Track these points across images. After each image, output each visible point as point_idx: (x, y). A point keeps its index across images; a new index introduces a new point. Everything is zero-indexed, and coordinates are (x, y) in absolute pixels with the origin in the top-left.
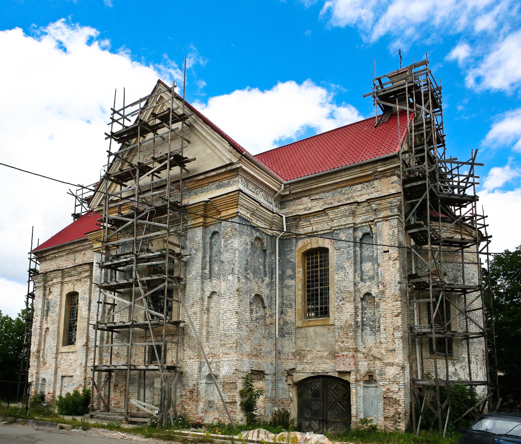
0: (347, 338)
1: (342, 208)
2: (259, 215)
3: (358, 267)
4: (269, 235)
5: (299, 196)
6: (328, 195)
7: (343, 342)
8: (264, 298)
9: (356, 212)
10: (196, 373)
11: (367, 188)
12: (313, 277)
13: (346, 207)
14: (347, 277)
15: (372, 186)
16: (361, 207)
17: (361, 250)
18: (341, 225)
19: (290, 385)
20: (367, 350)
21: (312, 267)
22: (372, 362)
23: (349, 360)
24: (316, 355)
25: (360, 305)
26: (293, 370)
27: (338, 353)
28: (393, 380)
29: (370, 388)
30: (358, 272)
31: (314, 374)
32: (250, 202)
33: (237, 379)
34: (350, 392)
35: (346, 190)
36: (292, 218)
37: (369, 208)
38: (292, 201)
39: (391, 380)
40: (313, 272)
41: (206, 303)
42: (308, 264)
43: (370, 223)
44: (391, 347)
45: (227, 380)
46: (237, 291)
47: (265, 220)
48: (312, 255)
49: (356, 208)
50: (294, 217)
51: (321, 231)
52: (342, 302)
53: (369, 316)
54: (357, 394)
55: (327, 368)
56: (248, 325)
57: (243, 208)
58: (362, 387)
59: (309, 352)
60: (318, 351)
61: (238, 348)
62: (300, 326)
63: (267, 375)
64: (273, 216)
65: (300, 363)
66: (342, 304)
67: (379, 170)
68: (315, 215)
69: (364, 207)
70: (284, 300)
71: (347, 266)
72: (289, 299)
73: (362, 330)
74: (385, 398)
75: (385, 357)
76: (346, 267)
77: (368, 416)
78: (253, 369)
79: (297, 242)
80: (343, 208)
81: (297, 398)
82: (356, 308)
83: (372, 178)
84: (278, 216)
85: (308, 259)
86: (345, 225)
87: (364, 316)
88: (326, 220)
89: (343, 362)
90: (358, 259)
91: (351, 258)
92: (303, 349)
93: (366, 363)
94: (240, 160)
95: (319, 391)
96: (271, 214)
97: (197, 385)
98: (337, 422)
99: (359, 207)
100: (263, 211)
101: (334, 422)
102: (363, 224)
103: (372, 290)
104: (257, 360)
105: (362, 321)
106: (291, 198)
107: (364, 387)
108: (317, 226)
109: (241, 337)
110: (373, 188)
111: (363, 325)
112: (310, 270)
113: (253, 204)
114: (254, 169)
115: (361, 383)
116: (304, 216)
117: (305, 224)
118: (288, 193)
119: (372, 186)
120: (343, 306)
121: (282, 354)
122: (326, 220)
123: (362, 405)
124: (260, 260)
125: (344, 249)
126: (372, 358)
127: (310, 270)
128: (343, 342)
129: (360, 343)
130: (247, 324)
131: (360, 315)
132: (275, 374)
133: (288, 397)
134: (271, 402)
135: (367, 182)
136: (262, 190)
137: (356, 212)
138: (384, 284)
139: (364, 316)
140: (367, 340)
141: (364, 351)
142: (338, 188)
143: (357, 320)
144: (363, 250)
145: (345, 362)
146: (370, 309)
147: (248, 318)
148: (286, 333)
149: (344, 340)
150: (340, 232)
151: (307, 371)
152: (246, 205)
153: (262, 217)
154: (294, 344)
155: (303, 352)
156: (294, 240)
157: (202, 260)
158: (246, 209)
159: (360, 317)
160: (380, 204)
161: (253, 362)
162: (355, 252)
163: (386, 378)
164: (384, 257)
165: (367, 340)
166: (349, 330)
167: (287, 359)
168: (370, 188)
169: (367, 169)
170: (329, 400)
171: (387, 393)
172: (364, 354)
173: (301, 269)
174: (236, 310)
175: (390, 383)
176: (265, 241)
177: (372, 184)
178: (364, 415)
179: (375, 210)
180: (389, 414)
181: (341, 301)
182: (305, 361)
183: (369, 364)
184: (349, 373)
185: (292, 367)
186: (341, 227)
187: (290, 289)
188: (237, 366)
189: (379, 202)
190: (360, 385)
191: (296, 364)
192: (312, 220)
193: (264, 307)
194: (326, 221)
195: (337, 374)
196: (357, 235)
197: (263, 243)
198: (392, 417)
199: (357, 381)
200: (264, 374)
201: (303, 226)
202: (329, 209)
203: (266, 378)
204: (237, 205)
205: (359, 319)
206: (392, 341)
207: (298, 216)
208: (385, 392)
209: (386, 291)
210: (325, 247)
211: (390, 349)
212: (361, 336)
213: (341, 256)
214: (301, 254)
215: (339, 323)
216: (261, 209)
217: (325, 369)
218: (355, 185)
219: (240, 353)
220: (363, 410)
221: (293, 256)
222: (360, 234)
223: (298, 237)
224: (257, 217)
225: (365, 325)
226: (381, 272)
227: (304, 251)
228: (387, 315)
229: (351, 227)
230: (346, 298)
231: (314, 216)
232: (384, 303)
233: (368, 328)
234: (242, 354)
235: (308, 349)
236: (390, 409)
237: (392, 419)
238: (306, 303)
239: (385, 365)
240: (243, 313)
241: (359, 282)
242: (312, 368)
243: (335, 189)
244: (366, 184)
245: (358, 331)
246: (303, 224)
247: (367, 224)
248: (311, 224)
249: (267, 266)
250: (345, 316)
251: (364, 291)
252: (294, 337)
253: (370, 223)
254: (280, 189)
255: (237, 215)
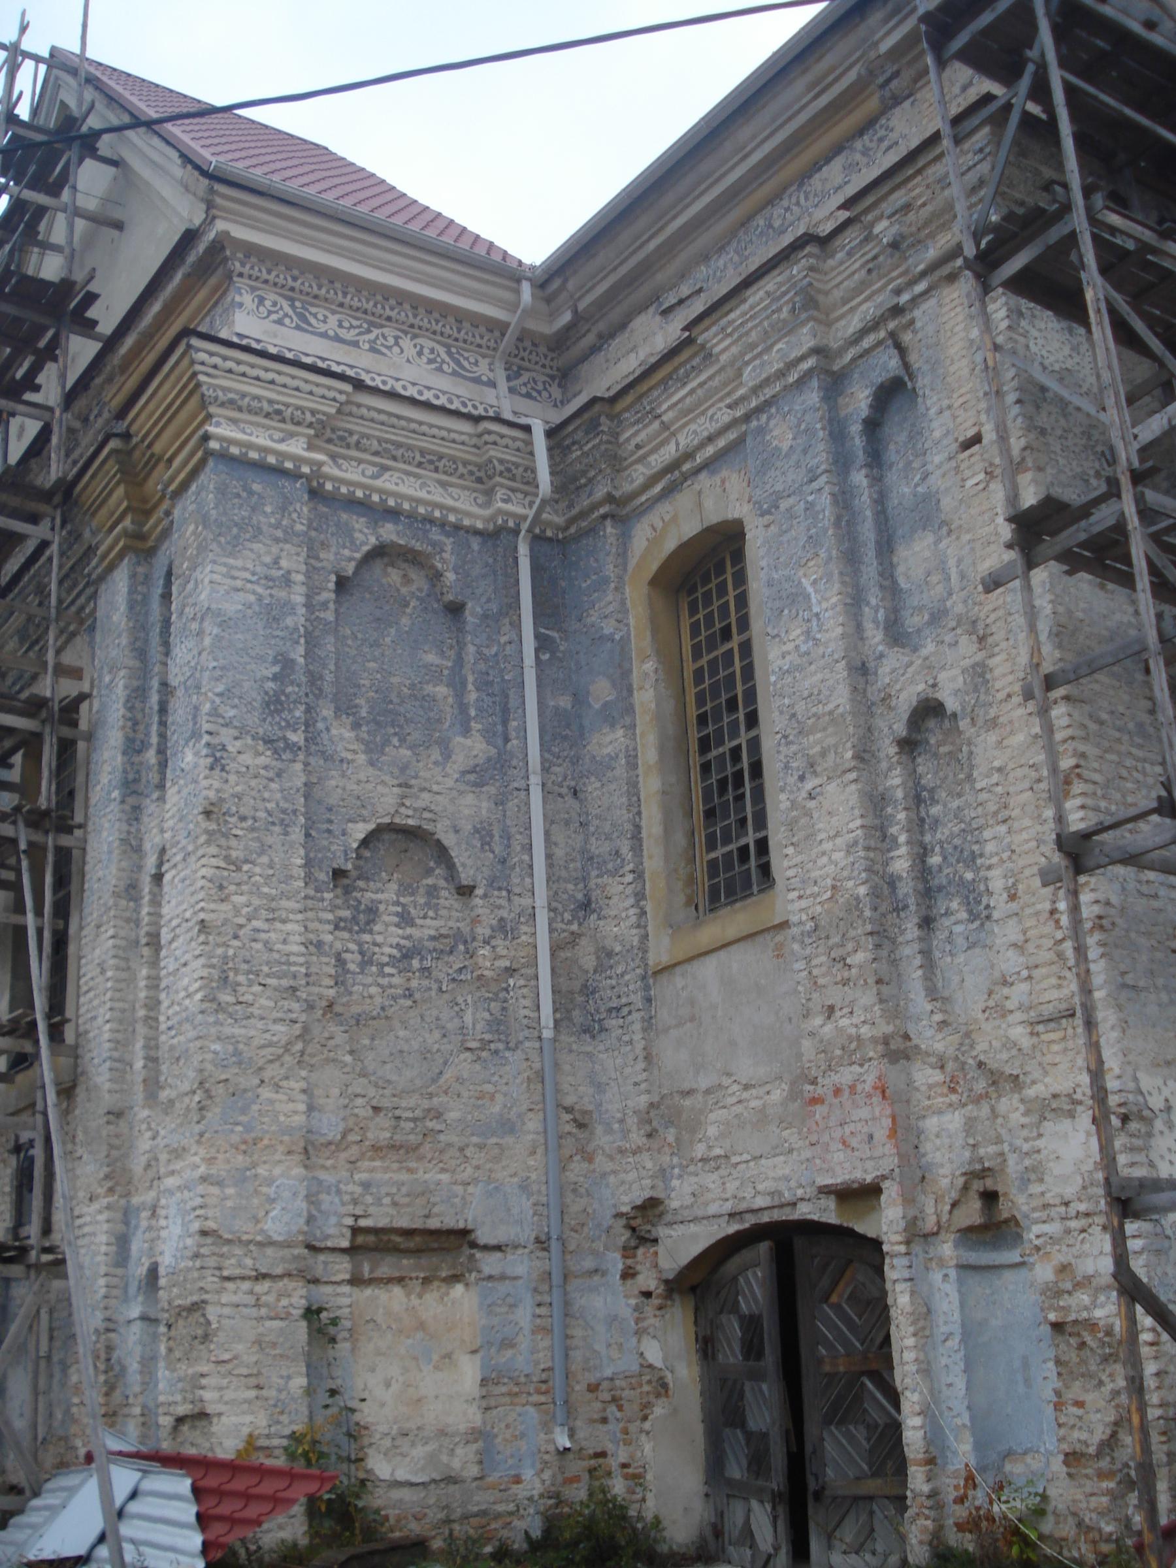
0: (845, 982)
1: (756, 296)
2: (380, 440)
3: (870, 570)
4: (477, 533)
5: (615, 315)
6: (721, 263)
7: (831, 1009)
8: (449, 840)
9: (827, 293)
10: (103, 1270)
11: (865, 160)
12: (715, 691)
13: (770, 284)
14: (817, 642)
15: (886, 143)
16: (840, 255)
17: (877, 480)
18: (767, 382)
19: (647, 1295)
20: (956, 1038)
21: (712, 645)
22: (985, 1110)
23: (864, 1113)
24: (739, 1109)
25: (895, 781)
26: (651, 1207)
27: (814, 1082)
28: (1083, 1207)
29: (1008, 1275)
30: (873, 601)
31: (742, 1221)
32: (280, 379)
33: (210, 1281)
34: (886, 1308)
35: (787, 209)
36: (578, 422)
37: (871, 249)
38: (600, 349)
39: (1072, 1211)
40: (713, 663)
41: (145, 910)
42: (695, 629)
43: (891, 325)
44: (1054, 994)
45: (179, 1296)
46: (207, 814)
47: (430, 461)
48: (706, 580)
49: (812, 269)
50: (586, 416)
51: (702, 446)
52: (809, 785)
53: (952, 836)
54: (925, 1313)
55: (787, 1179)
56: (294, 989)
57: (244, 416)
58: (953, 1273)
59: (711, 1100)
60: (747, 1087)
61: (214, 1114)
62: (665, 960)
63: (486, 1248)
64: (480, 436)
65: (681, 1166)
66: (811, 797)
67: (884, 47)
68: (669, 376)
69: (850, 254)
70: (593, 840)
71: (815, 582)
72: (607, 827)
73: (927, 923)
74: (1057, 1327)
75: (1032, 1066)
76: (810, 590)
77: (1008, 1454)
78: (363, 1223)
79: (625, 538)
80: (761, 293)
81: (696, 1370)
82: (876, 802)
83: (872, 104)
84: (505, 430)
85: (693, 610)
86: (781, 374)
87: (928, 838)
88: (716, 382)
89: (837, 1134)
90: (867, 531)
91: (825, 530)
92: (686, 1086)
93: (954, 1121)
94: (210, 205)
95: (760, 1316)
96: (466, 427)
97: (108, 1330)
98: (871, 1498)
99: (831, 262)
100: (399, 417)
101: (856, 1499)
102: (867, 343)
103: (943, 676)
104: (410, 1171)
105: (922, 870)
106: (590, 339)
107: (963, 1267)
108: (693, 427)
109: (237, 1053)
110: (890, 148)
111: (928, 893)
112: (704, 661)
113: (308, 387)
114: (306, 231)
115: (947, 1249)
116: (629, 399)
117: (642, 436)
118: (567, 317)
119: (886, 143)
120: (812, 804)
121: (599, 1130)
122: (716, 382)
123: (960, 1384)
124: (431, 658)
125: (791, 500)
126: (980, 1086)
127: (704, 661)
128: (831, 1009)
129: (920, 1002)
130: (285, 983)
131: (902, 839)
132: (542, 1243)
133: (635, 1368)
134: (535, 1398)
135: (861, 132)
136: (413, 331)
137: (827, 293)
138: (980, 626)
139: (928, 838)
140: (956, 979)
141: (939, 1047)
142: (750, 218)
143: (890, 869)
144: (892, 477)
145: (847, 1129)
146: (950, 793)
147: (296, 948)
148: (610, 1010)
149: (835, 995)
150: (769, 419)
151: (713, 1209)
152: (258, 398)
153: (410, 448)
154: (641, 1065)
155: (687, 1102)
156: (609, 530)
157: (131, 709)
158: (267, 415)
159: (903, 850)
160: (907, 208)
161: (366, 1185)
162: (844, 499)
163: (1049, 1198)
164: (967, 473)
165: (956, 979)
166: (852, 933)
167: (621, 1151)
168: (879, 154)
169: (833, 69)
170: (827, 1368)
171: (1059, 1293)
172: (942, 1067)
173: (649, 666)
174: (202, 916)
175: (1068, 1231)
176: (447, 560)
177: (882, 133)
178: (980, 1446)
179: (895, 245)
180: (1084, 1436)
181: (802, 778)
182: (700, 1150)
183: (970, 1125)
184: (867, 1194)
185: (639, 1195)
186: (768, 392)
187: (609, 774)
188: (210, 1213)
189: (899, 198)
190: (941, 1263)
191: (663, 1173)
192: (665, 406)
193: (465, 891)
194: (717, 390)
195: (831, 1203)
196: (850, 409)
197: (438, 575)
198: (1099, 1455)
199: (916, 1235)
200: (474, 1245)
201: (638, 447)
202: (707, 322)
203: (487, 1270)
204: (203, 405)
205: (901, 864)
206: (1050, 956)
207: (597, 408)
208: (1054, 1292)
209: (991, 662)
210: (730, 517)
211: (1047, 1010)
212: (918, 961)
213: (785, 538)
214: (645, 589)
215: (804, 903)
216: (380, 411)
217: (782, 1186)
218: (816, 166)
219: (235, 1139)
220: (966, 1419)
221: (611, 608)
222: (859, 400)
223: (628, 509)
224: (376, 453)
225: (940, 889)
226: (960, 561)
227: (655, 567)
228: (1012, 802)
229: (809, 373)
230: (823, 754)
231: (664, 381)
232: (992, 738)
233: (954, 905)
234: (249, 1145)
235: (704, 1083)
236: (1089, 1397)
237: (1104, 1464)
238: (700, 838)
239: (1034, 1118)
240: (256, 924)
241: (881, 656)
242: (731, 1187)
243: (745, 222)
244: (858, 145)
245: (902, 932)
246: (638, 439)
247: (882, 334)
248: (665, 427)
249: (470, 679)
250: (825, 860)
251: (907, 698)
252: (637, 1026)
253: (891, 325)
254: (513, 307)
255: (209, 453)
